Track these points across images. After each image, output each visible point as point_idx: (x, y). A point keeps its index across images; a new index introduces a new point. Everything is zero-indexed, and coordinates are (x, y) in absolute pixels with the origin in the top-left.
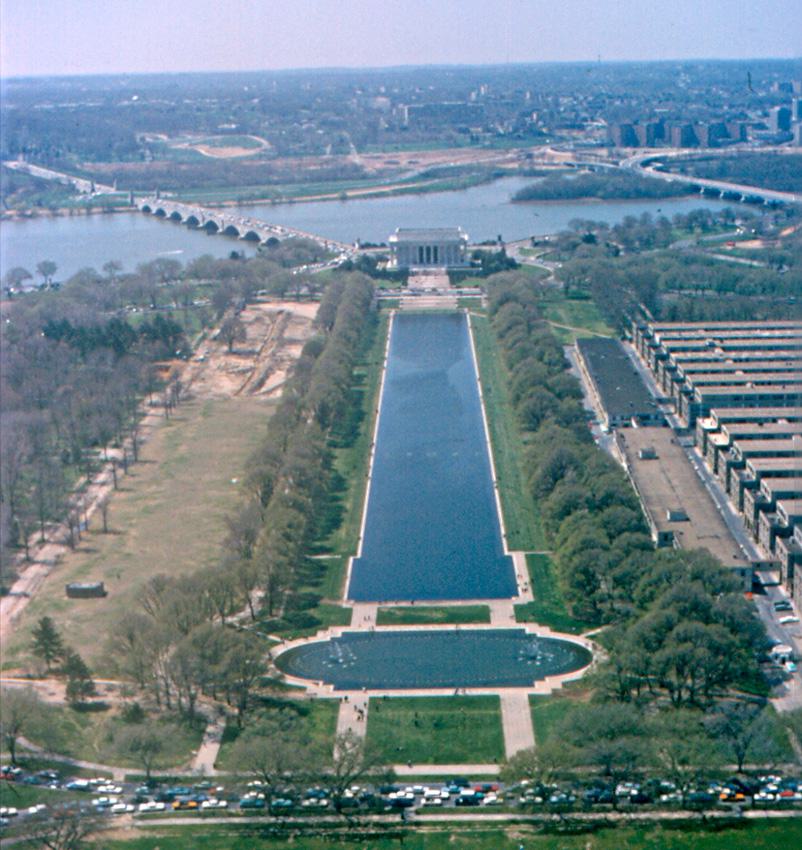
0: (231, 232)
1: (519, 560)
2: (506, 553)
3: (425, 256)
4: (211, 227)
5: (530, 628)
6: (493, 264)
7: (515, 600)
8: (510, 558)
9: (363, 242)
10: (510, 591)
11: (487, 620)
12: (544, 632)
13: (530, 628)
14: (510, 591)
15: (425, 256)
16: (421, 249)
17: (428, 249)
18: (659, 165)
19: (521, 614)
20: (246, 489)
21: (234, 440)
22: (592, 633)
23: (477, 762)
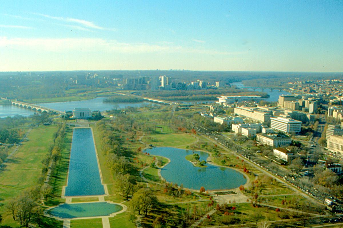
0: (35, 110)
1: (105, 186)
2: (102, 184)
3: (83, 114)
4: (30, 108)
5: (108, 202)
6: (98, 117)
7: (105, 195)
8: (103, 185)
9: (66, 111)
10: (103, 193)
11: (98, 201)
12: (112, 203)
13: (108, 202)
14: (103, 193)
15: (83, 114)
16: (80, 113)
17: (82, 113)
18: (135, 94)
19: (106, 199)
20: (41, 180)
21: (128, 91)
22: (123, 202)
23: (75, 202)
